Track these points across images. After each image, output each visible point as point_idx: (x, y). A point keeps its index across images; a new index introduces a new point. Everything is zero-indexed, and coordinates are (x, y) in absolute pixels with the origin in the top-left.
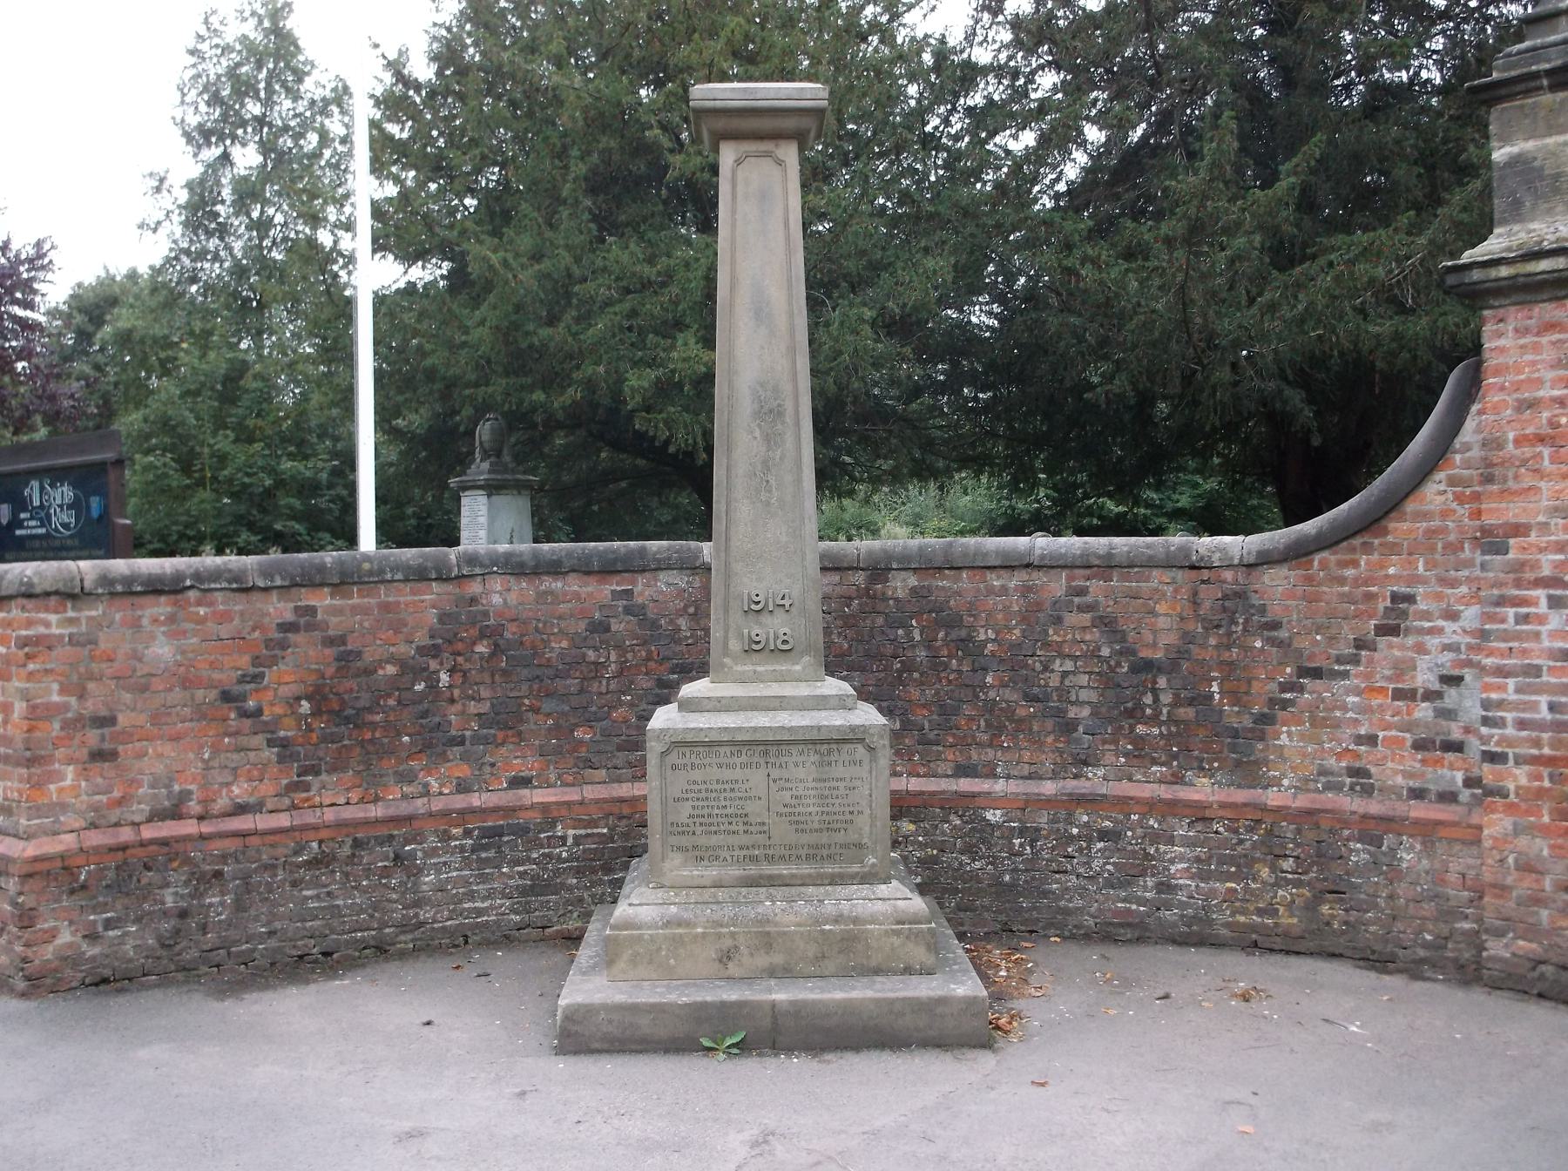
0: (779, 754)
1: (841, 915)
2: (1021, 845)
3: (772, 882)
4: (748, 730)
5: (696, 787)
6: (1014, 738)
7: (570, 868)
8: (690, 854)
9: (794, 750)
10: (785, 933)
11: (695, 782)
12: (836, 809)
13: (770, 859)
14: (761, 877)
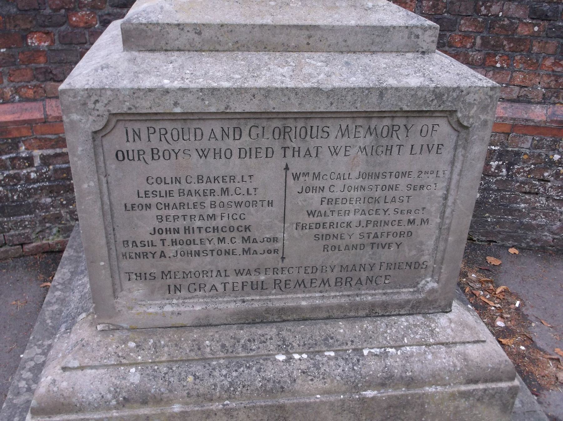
0: (308, 133)
1: (391, 377)
2: (498, 167)
3: (282, 316)
4: (254, 93)
5: (163, 188)
6: (510, 58)
7: (42, 188)
8: (159, 283)
9: (333, 127)
10: (307, 405)
11: (160, 180)
12: (391, 216)
13: (282, 286)
14: (268, 311)
